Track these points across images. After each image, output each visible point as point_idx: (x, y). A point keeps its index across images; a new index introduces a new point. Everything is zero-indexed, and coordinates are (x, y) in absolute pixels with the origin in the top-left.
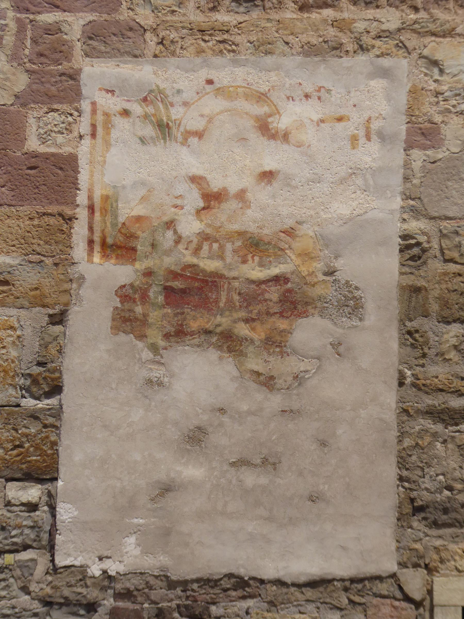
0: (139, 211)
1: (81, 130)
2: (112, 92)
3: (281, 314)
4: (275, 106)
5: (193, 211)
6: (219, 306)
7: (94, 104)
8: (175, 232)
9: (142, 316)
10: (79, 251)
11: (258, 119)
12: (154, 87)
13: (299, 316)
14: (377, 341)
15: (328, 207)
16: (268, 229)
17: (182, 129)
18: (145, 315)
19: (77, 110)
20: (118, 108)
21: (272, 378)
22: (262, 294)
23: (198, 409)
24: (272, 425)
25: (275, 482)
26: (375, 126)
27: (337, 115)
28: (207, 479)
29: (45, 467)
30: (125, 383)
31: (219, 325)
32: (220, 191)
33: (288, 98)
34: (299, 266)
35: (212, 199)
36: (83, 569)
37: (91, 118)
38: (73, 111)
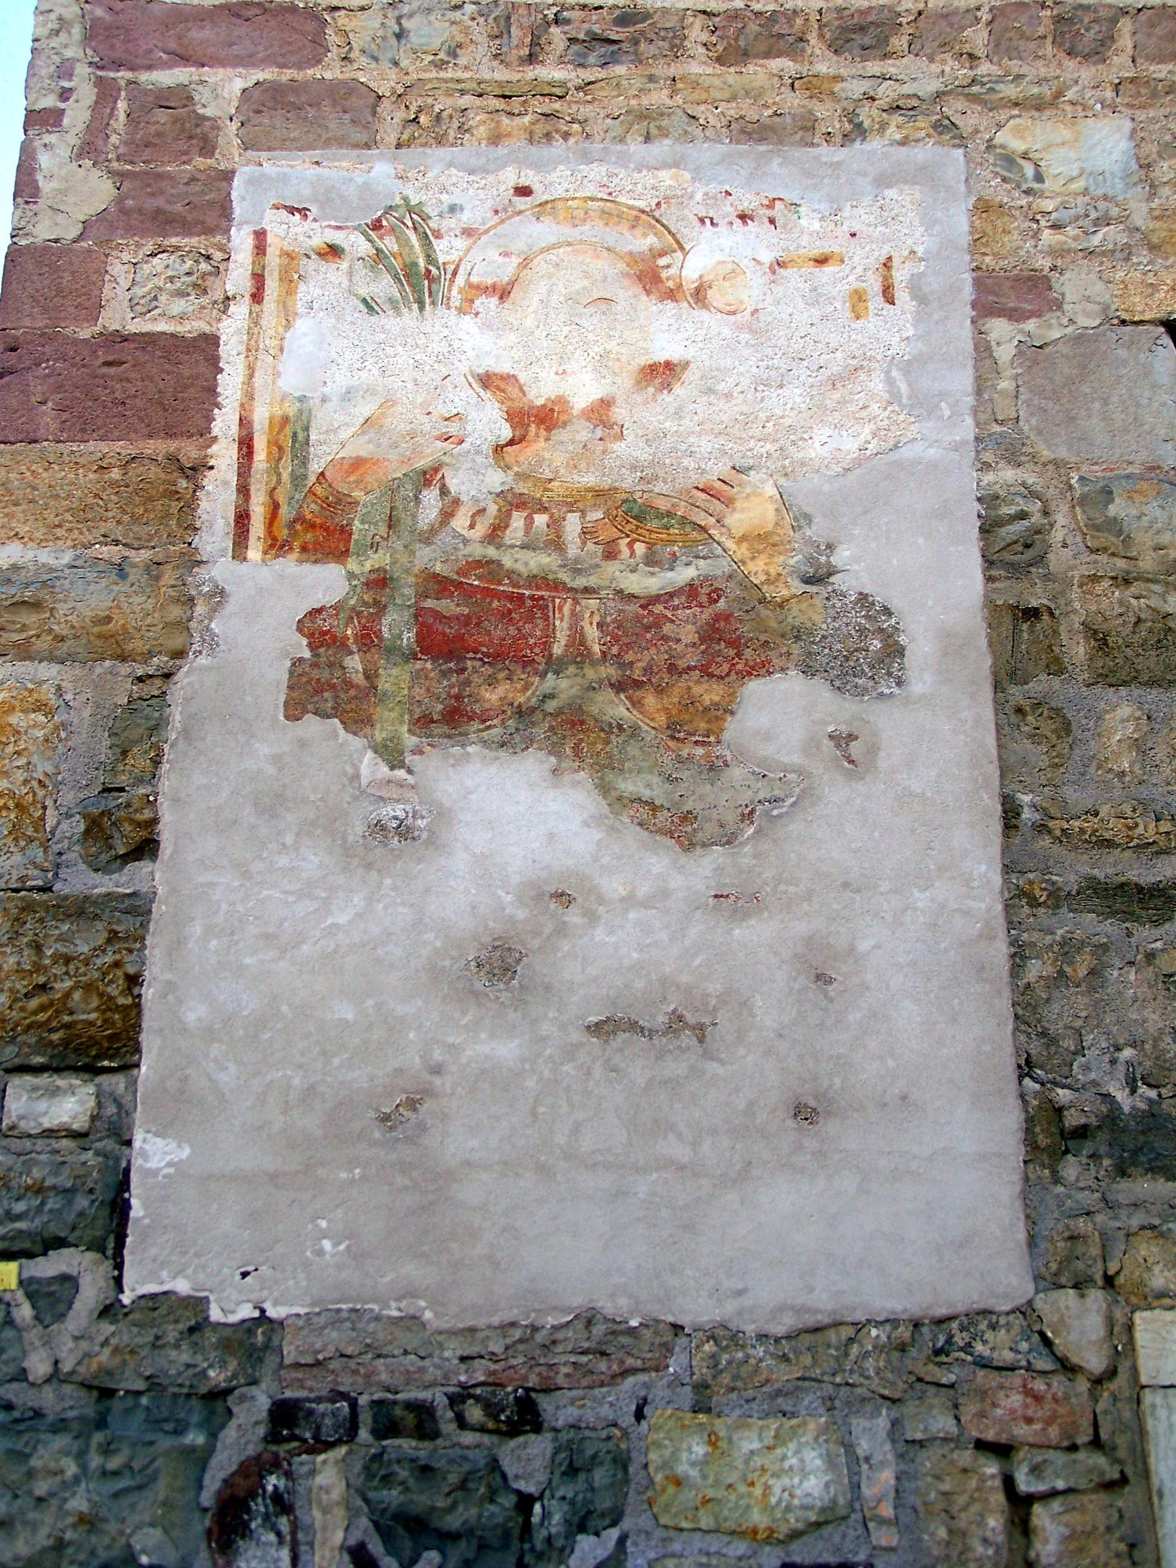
0: (361, 448)
1: (228, 287)
2: (303, 212)
3: (706, 672)
4: (673, 235)
5: (487, 449)
6: (551, 655)
7: (260, 236)
8: (444, 491)
9: (361, 676)
10: (214, 536)
11: (632, 258)
12: (398, 201)
13: (753, 671)
14: (938, 735)
15: (806, 436)
16: (665, 482)
17: (460, 280)
18: (370, 675)
19: (222, 249)
20: (317, 242)
21: (687, 817)
22: (657, 625)
23: (501, 893)
24: (693, 932)
25: (704, 1072)
26: (900, 276)
27: (816, 253)
28: (527, 1067)
29: (111, 1038)
30: (318, 832)
31: (552, 696)
32: (550, 405)
33: (702, 221)
34: (744, 563)
35: (534, 420)
36: (198, 1304)
37: (254, 262)
38: (211, 251)
